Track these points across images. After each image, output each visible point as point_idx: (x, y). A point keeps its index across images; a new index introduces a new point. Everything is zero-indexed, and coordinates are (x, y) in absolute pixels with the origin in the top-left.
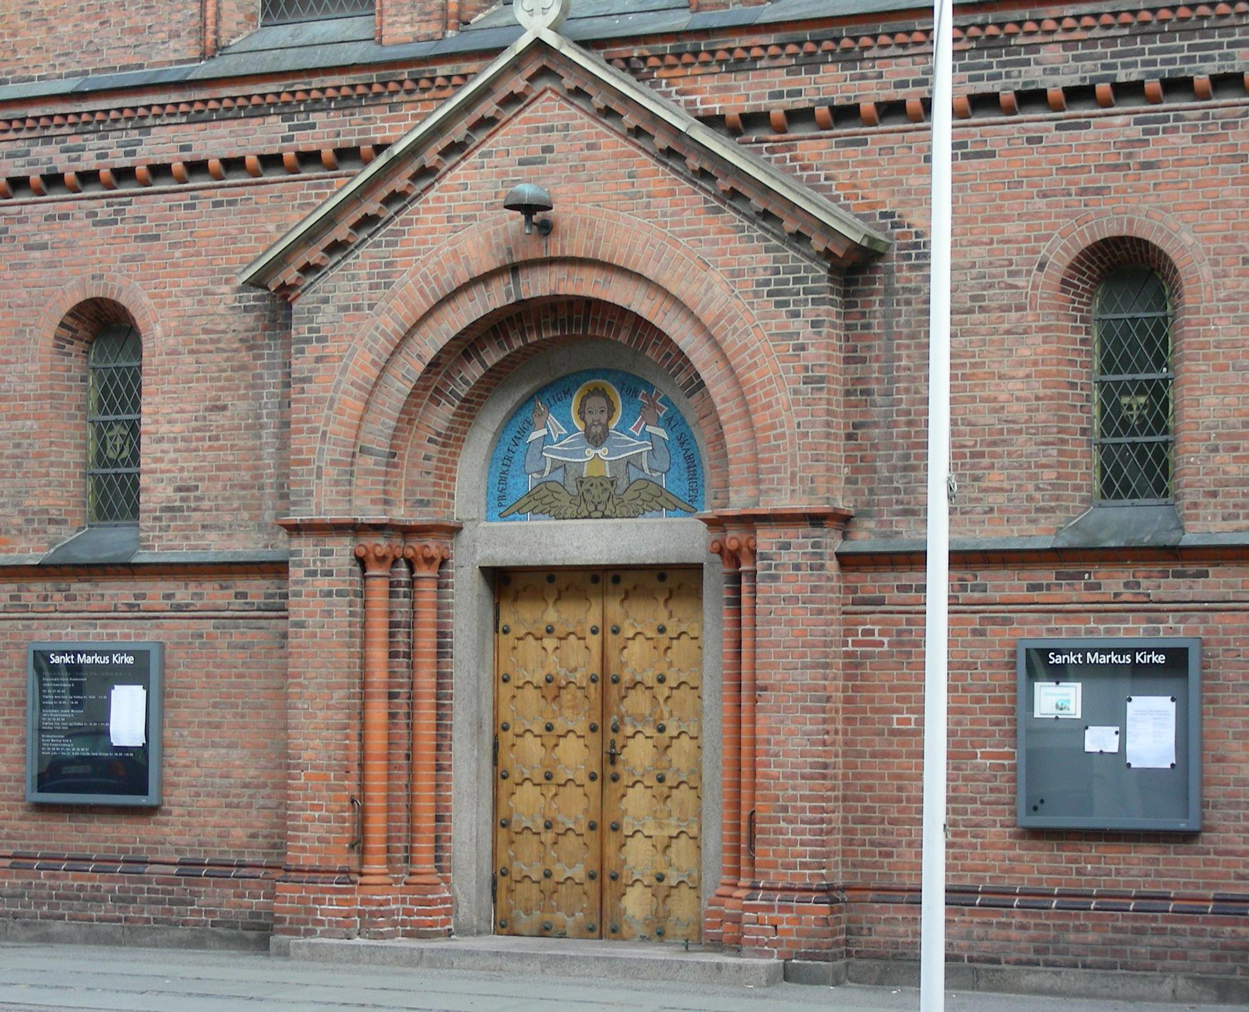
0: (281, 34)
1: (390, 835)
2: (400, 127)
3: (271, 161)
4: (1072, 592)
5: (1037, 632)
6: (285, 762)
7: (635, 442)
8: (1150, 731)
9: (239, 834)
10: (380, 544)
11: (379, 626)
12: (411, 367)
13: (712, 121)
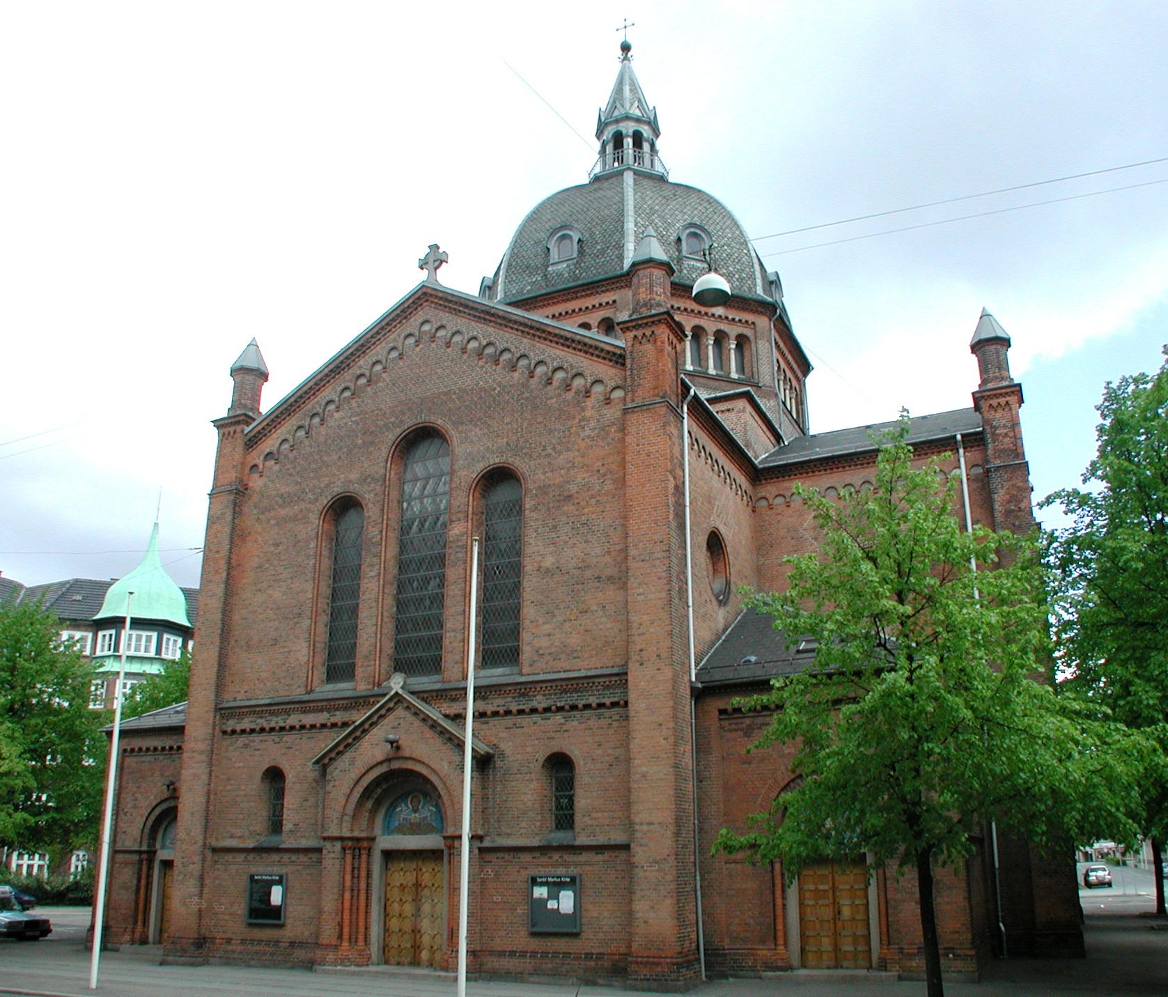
0: (330, 687)
1: (351, 932)
2: (359, 717)
3: (323, 726)
4: (544, 859)
5: (533, 872)
6: (321, 912)
7: (427, 811)
8: (566, 902)
9: (307, 933)
10: (350, 843)
11: (349, 869)
12: (359, 790)
13: (446, 716)
